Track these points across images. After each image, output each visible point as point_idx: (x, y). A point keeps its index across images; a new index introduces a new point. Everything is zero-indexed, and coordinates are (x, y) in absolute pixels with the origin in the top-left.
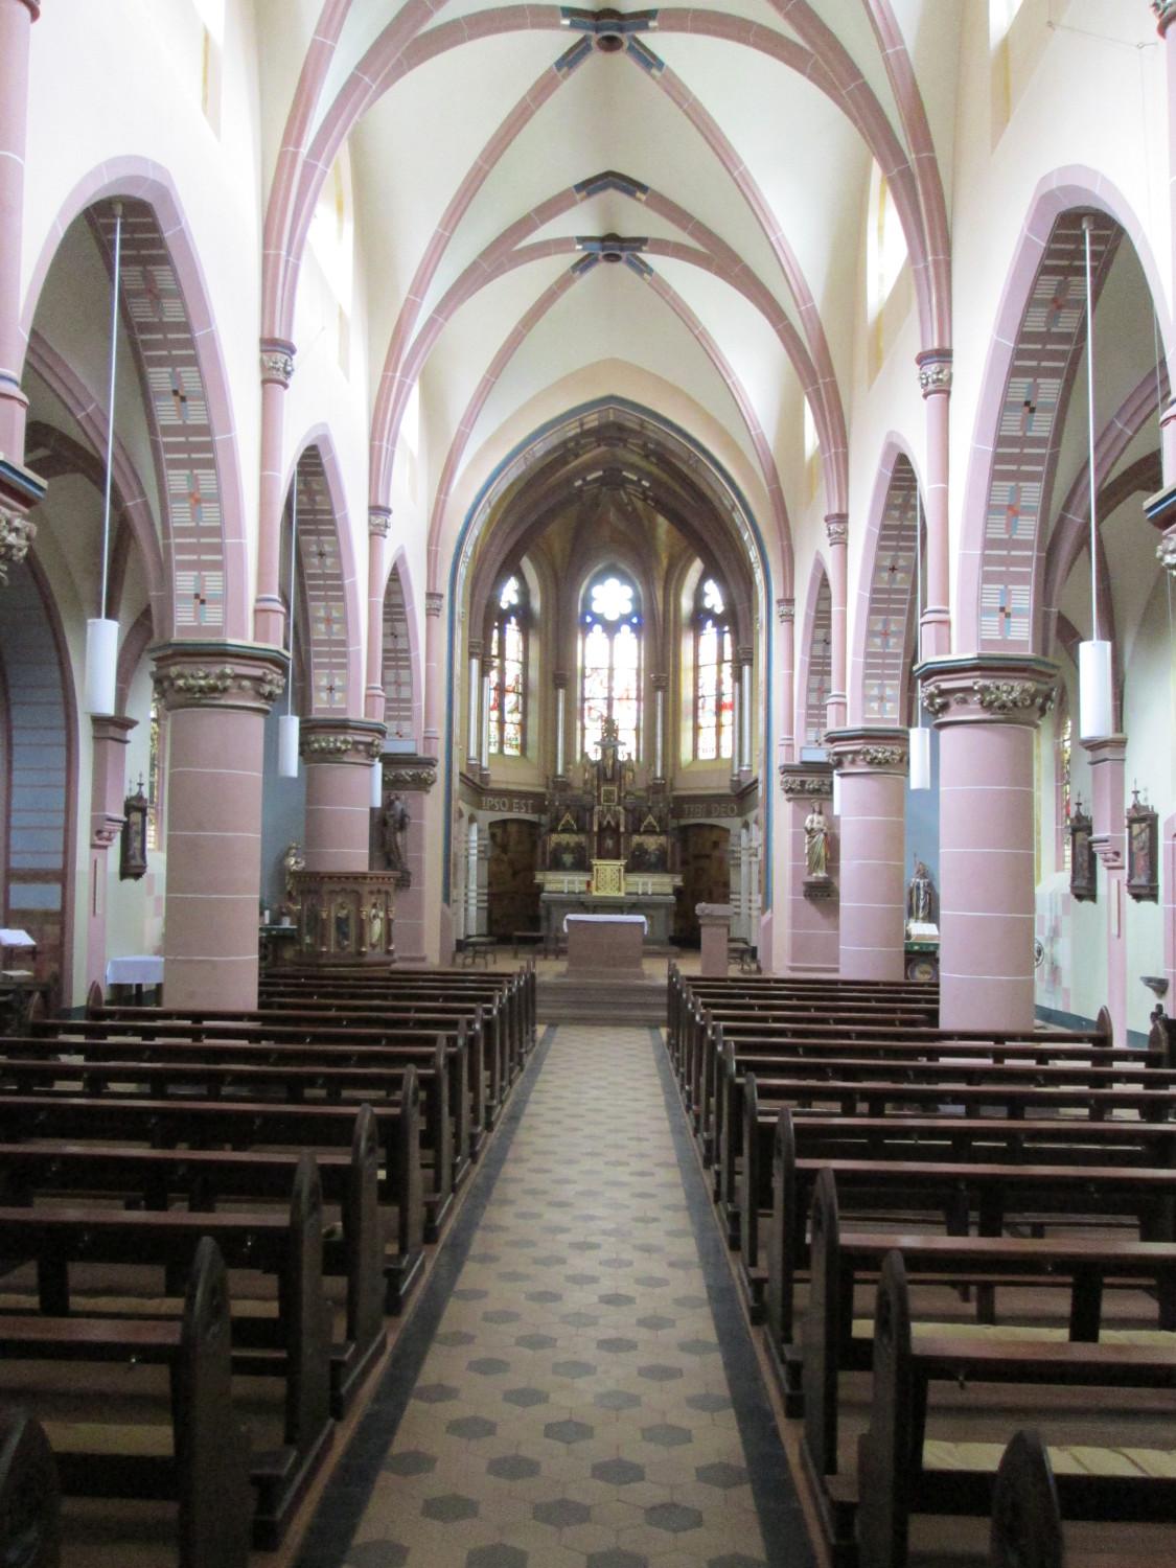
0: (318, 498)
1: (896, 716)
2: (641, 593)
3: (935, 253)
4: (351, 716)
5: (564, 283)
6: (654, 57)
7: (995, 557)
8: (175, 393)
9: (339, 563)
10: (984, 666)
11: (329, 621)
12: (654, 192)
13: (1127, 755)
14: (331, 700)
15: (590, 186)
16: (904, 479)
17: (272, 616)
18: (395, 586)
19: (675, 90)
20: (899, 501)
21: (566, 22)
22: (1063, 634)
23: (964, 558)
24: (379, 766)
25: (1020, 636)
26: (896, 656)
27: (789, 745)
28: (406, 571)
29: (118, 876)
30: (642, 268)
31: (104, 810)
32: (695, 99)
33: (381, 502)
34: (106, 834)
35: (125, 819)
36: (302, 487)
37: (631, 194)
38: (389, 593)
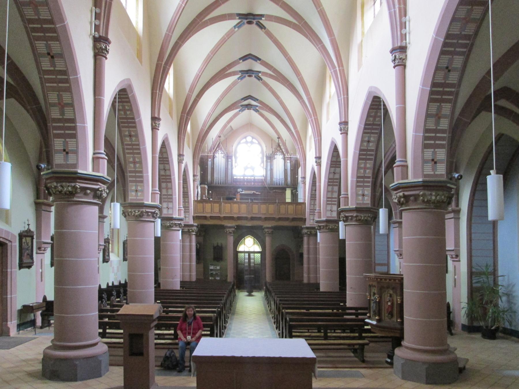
0: (128, 113)
1: (369, 202)
2: (265, 149)
3: (344, 95)
4: (174, 216)
5: (229, 34)
6: (264, 26)
7: (360, 179)
8: (49, 54)
9: (188, 190)
10: (358, 210)
11: (134, 163)
12: (267, 15)
13: (461, 216)
14: (136, 195)
15: (245, 58)
16: (376, 101)
17: (156, 195)
18: (164, 150)
19: (270, 35)
20: (373, 114)
21: (241, 61)
22: (376, 203)
23: (352, 181)
24: (159, 221)
25: (367, 201)
26: (369, 177)
27: (345, 197)
28: (169, 144)
29: (50, 265)
30: (262, 27)
31: (41, 239)
32: (275, 38)
33: (181, 153)
34: (43, 249)
35: (52, 242)
36: (121, 108)
37: (256, 61)
38: (161, 152)
